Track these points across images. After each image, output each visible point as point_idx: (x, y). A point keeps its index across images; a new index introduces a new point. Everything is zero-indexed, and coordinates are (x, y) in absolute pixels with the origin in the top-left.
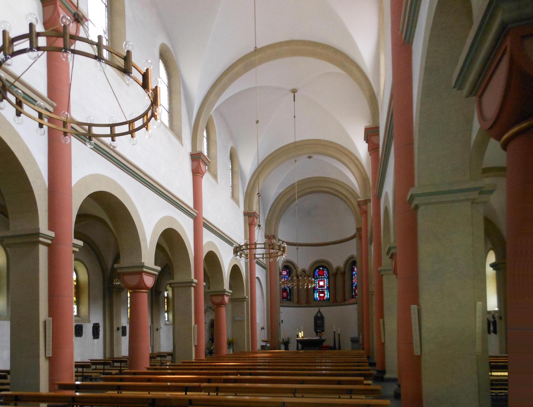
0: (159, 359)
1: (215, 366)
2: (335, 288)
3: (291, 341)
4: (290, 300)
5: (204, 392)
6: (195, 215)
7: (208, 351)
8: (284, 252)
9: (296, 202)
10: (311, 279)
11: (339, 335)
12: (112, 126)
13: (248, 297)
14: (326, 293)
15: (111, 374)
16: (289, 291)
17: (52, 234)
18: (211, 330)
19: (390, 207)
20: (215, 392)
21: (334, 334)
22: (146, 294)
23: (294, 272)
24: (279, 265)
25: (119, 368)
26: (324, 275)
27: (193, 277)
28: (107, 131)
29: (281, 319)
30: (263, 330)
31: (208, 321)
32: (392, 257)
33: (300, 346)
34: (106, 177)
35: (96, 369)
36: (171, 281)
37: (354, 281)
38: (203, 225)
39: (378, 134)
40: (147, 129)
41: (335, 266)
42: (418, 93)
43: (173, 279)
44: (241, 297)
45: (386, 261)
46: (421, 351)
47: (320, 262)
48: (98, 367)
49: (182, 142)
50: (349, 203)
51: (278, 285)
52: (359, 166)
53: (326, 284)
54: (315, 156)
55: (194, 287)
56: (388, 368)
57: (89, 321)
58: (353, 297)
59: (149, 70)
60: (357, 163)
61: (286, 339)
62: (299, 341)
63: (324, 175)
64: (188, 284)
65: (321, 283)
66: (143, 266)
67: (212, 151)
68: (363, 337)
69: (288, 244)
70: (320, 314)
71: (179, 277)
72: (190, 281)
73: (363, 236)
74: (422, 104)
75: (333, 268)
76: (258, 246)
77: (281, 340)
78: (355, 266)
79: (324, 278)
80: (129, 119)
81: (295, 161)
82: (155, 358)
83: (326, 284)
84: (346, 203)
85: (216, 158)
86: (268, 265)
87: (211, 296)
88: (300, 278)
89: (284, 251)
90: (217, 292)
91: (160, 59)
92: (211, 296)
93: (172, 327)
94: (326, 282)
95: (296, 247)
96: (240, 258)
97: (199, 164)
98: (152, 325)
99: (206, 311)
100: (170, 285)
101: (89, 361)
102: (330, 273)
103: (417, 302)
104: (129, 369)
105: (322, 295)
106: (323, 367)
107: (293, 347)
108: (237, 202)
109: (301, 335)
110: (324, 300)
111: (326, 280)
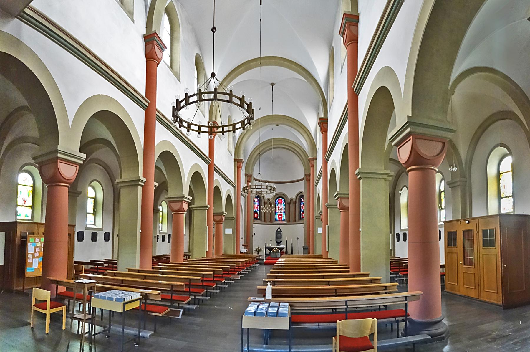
4: (259, 219)
6: (147, 105)
14: (283, 215)
17: (145, 180)
26: (282, 203)
27: (207, 204)
38: (157, 118)
44: (220, 211)
50: (300, 157)
55: (142, 186)
60: (303, 150)
71: (172, 193)
87: (170, 203)
102: (286, 202)
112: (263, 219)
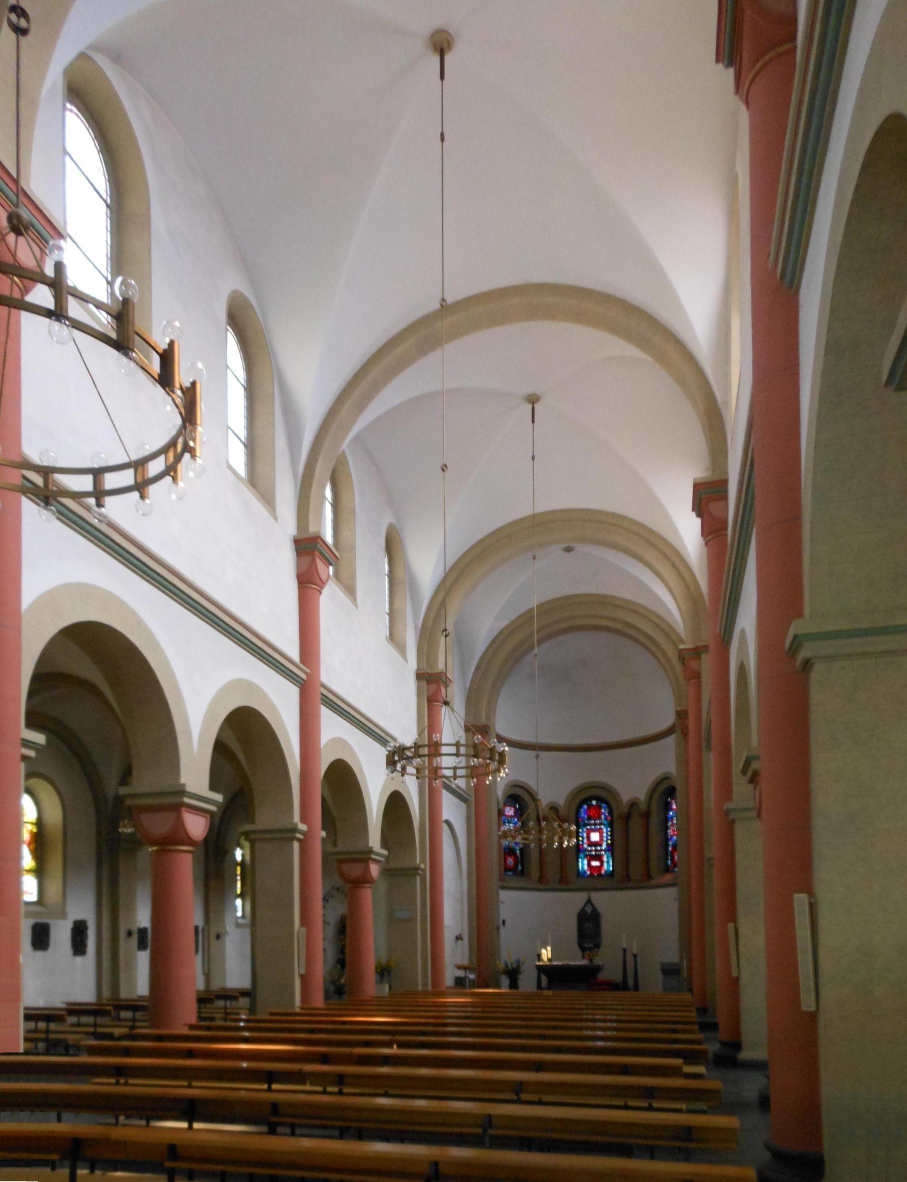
0: (221, 1003)
1: (344, 1023)
2: (626, 851)
3: (523, 968)
4: (522, 873)
5: (312, 1084)
6: (304, 676)
7: (332, 988)
8: (503, 765)
9: (536, 651)
10: (569, 827)
11: (635, 956)
12: (97, 473)
13: (426, 866)
14: (605, 859)
15: (111, 1037)
16: (521, 853)
18: (341, 940)
19: (749, 666)
20: (335, 1086)
21: (625, 955)
22: (188, 859)
23: (531, 810)
24: (496, 793)
25: (131, 1024)
26: (600, 818)
27: (418, 861)
28: (85, 483)
29: (502, 917)
30: (459, 942)
31: (333, 918)
32: (754, 779)
33: (544, 980)
34: (102, 590)
35: (78, 1025)
36: (248, 827)
37: (670, 832)
38: (322, 699)
39: (725, 498)
40: (175, 479)
41: (626, 797)
42: (812, 397)
43: (253, 822)
44: (406, 864)
45: (741, 788)
46: (817, 999)
47: (591, 787)
48: (84, 1019)
49: (275, 511)
50: (658, 654)
51: (495, 838)
52: (682, 569)
53: (605, 839)
54: (580, 548)
55: (300, 840)
56: (746, 1039)
57: (63, 915)
58: (667, 870)
59: (176, 345)
60: (678, 563)
61: (512, 964)
62: (542, 970)
63: (602, 591)
64: (288, 835)
65: (595, 837)
66: (182, 792)
67: (345, 534)
68: (690, 961)
69: (511, 744)
70: (591, 907)
71: (265, 819)
72: (289, 826)
73: (692, 728)
74: (821, 422)
75: (622, 802)
76: (444, 750)
77: (501, 966)
78: (673, 798)
79: (600, 824)
80: (134, 457)
81: (534, 558)
82: (210, 1001)
83: (605, 839)
84: (652, 653)
85: (353, 548)
86: (473, 795)
88: (544, 824)
89: (502, 762)
90: (352, 853)
91: (230, 325)
92: (341, 862)
93: (248, 931)
94: (605, 835)
95: (532, 753)
96: (403, 775)
97: (313, 561)
98: (206, 927)
99: (325, 899)
100: (247, 834)
101: (64, 1006)
102: (615, 814)
103: (808, 889)
104: (150, 1027)
105: (595, 863)
106: (599, 1033)
107: (528, 982)
108: (401, 649)
109: (546, 954)
110: (600, 875)
111: (605, 830)
112: (535, 872)
